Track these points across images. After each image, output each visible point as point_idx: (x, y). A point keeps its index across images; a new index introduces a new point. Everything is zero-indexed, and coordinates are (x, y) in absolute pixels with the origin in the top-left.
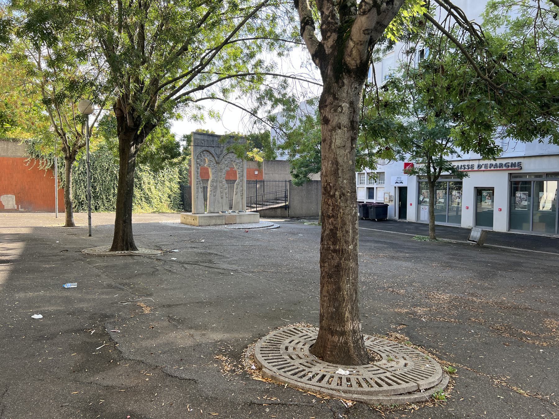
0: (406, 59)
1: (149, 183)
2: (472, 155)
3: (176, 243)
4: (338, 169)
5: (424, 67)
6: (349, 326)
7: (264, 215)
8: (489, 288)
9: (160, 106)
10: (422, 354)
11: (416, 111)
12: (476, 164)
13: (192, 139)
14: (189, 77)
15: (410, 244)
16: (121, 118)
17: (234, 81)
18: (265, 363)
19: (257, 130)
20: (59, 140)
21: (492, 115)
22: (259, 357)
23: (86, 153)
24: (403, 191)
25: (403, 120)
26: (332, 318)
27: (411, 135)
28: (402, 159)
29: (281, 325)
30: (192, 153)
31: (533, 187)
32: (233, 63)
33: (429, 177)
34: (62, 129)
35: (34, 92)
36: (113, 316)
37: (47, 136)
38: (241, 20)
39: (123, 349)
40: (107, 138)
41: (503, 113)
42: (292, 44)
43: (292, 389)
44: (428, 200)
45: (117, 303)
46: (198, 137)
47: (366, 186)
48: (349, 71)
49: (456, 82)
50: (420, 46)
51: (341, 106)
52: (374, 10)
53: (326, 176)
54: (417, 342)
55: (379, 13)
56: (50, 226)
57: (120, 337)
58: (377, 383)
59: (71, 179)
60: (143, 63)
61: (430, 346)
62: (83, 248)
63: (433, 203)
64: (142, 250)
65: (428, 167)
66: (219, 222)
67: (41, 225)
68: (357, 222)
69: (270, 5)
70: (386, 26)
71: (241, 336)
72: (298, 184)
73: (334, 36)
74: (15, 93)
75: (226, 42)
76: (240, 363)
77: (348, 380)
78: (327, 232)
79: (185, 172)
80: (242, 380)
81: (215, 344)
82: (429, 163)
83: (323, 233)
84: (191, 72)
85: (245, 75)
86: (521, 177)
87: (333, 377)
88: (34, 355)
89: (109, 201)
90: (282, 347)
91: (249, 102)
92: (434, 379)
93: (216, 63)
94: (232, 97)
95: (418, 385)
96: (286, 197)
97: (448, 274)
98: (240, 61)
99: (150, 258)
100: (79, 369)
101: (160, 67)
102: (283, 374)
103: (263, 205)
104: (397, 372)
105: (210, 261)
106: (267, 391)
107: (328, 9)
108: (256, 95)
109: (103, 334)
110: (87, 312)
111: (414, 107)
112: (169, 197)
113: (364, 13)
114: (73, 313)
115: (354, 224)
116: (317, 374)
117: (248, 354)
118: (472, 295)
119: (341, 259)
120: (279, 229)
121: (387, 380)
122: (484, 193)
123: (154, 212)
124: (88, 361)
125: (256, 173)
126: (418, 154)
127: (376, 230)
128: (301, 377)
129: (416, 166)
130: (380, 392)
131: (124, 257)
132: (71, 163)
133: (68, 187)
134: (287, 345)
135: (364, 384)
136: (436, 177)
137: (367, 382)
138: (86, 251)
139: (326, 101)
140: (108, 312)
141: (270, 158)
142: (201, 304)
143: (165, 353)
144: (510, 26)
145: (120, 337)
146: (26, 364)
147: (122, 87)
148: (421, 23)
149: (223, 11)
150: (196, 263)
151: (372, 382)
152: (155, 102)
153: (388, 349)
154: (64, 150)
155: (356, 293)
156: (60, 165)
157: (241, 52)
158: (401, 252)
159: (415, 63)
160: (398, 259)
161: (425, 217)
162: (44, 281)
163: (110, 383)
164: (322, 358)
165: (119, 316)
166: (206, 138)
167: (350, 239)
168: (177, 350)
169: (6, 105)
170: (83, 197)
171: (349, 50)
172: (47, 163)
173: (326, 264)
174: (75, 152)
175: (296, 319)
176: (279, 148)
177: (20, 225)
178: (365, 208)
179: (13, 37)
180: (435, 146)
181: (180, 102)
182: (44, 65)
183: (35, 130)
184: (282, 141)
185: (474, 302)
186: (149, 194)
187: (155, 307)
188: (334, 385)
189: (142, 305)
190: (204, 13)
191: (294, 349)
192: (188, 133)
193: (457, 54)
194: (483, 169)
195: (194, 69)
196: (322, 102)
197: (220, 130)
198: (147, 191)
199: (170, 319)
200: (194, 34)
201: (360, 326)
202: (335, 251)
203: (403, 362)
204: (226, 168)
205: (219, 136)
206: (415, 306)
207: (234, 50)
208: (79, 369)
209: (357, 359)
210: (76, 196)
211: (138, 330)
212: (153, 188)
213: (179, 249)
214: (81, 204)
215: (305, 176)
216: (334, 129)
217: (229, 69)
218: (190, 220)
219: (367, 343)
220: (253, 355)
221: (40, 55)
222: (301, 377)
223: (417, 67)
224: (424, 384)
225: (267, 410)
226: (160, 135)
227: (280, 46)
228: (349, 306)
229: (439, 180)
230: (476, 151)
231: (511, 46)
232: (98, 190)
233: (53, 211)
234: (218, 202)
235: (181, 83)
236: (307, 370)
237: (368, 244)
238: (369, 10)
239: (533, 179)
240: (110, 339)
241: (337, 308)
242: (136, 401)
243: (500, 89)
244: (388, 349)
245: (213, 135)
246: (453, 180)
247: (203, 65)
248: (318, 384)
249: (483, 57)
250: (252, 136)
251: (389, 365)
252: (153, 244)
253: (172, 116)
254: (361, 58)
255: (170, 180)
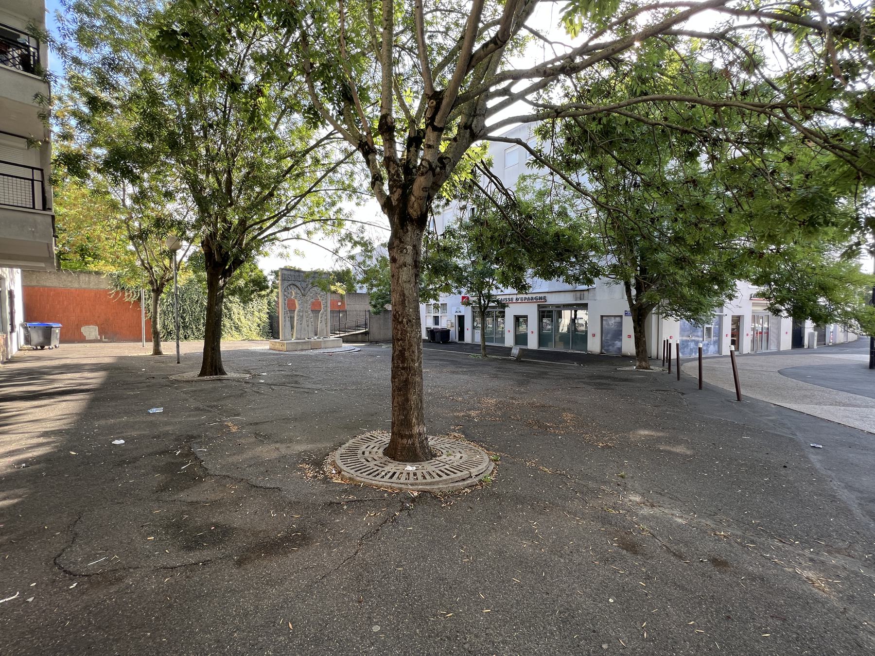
0: (459, 214)
1: (238, 314)
2: (510, 290)
3: (264, 367)
4: (405, 300)
5: (474, 221)
6: (416, 430)
7: (346, 340)
8: (524, 393)
9: (247, 244)
10: (474, 448)
11: (469, 255)
12: (515, 297)
13: (280, 274)
14: (276, 219)
15: (467, 361)
16: (209, 255)
17: (317, 225)
18: (344, 468)
19: (339, 267)
20: (146, 274)
21: (524, 260)
22: (339, 463)
23: (174, 286)
24: (461, 319)
25: (460, 263)
26: (402, 424)
27: (466, 274)
28: (460, 293)
29: (359, 434)
30: (280, 286)
31: (555, 315)
32: (316, 210)
33: (480, 308)
34: (148, 263)
35: (118, 227)
36: (200, 436)
37: (133, 270)
38: (323, 173)
39: (209, 466)
40: (195, 272)
41: (531, 259)
42: (369, 197)
43: (367, 486)
44: (480, 325)
45: (204, 424)
46: (286, 272)
47: (433, 315)
48: (412, 220)
49: (497, 234)
50: (470, 205)
51: (406, 248)
52: (430, 173)
53: (395, 305)
54: (470, 438)
55: (434, 175)
56: (136, 355)
57: (206, 456)
58: (438, 474)
59: (159, 310)
60: (231, 205)
61: (481, 441)
62: (171, 375)
63: (483, 328)
64: (230, 374)
65: (480, 300)
66: (305, 347)
67: (126, 354)
68: (421, 344)
69: (348, 162)
70: (440, 186)
71: (323, 446)
72: (376, 313)
73: (399, 191)
74: (99, 227)
75: (309, 191)
76: (322, 469)
77: (415, 474)
78: (396, 353)
79: (274, 303)
80: (323, 484)
81: (299, 455)
82: (480, 297)
83: (394, 353)
84: (277, 215)
85: (327, 220)
86: (546, 307)
87: (402, 473)
88: (113, 480)
89: (199, 330)
90: (360, 452)
91: (332, 243)
92: (482, 467)
93: (301, 208)
94: (315, 238)
95: (470, 473)
96: (366, 324)
97: (495, 383)
98: (323, 208)
99: (238, 381)
100: (163, 488)
101: (249, 209)
102: (360, 475)
103: (345, 332)
104: (454, 464)
105: (296, 382)
106: (345, 491)
107: (394, 169)
108: (337, 238)
109: (189, 454)
110: (172, 434)
111: (468, 252)
112: (259, 326)
113: (422, 174)
114: (158, 437)
115: (418, 345)
116: (389, 472)
117: (329, 461)
118: (512, 398)
119: (408, 375)
120: (360, 352)
121: (446, 471)
122: (521, 320)
123: (244, 340)
124: (172, 480)
125: (340, 304)
126: (472, 290)
127: (441, 350)
128: (375, 476)
129: (471, 299)
130: (441, 481)
131: (213, 382)
132: (159, 295)
133: (155, 318)
134: (363, 450)
135: (428, 477)
136: (486, 308)
137: (430, 474)
138: (174, 378)
139: (393, 243)
140: (195, 433)
141: (351, 291)
142: (287, 420)
143: (251, 466)
144: (535, 194)
145: (206, 456)
146: (104, 489)
147: (209, 226)
148: (470, 186)
149: (306, 165)
150: (283, 384)
151: (434, 475)
152: (242, 240)
153: (448, 446)
154: (151, 283)
155: (421, 402)
156: (147, 296)
157: (324, 201)
158: (460, 367)
159: (467, 216)
160: (457, 373)
161: (478, 339)
162: (127, 407)
163: (194, 499)
164: (394, 458)
165: (206, 436)
166: (292, 273)
167: (416, 358)
168: (262, 464)
169: (88, 238)
170: (171, 327)
171: (411, 203)
172: (133, 295)
173: (396, 380)
174: (162, 285)
175: (372, 428)
176: (358, 283)
177: (103, 355)
178: (431, 333)
179: (90, 172)
180: (483, 283)
181: (266, 241)
182: (128, 202)
183: (119, 263)
184: (360, 277)
185: (513, 404)
186: (239, 323)
187: (242, 425)
188: (403, 480)
189: (230, 424)
190: (289, 165)
191: (370, 453)
192: (277, 269)
193: (497, 212)
194: (519, 301)
195: (280, 213)
196: (391, 246)
197: (306, 266)
198: (237, 321)
199: (257, 435)
200: (279, 182)
201: (425, 429)
202: (403, 368)
203: (459, 455)
204: (312, 300)
205: (304, 272)
206: (469, 410)
207: (317, 199)
208: (163, 488)
209: (422, 457)
210: (164, 326)
211: (225, 448)
212: (242, 318)
213: (266, 372)
214: (170, 333)
215: (382, 306)
216: (401, 267)
217: (312, 214)
218: (278, 346)
219: (431, 443)
220: (334, 461)
221: (124, 193)
222: (375, 476)
223: (468, 221)
224: (474, 471)
225: (345, 507)
226: (248, 270)
227: (358, 198)
228: (416, 414)
229: (488, 310)
230: (513, 287)
231: (535, 208)
232: (187, 320)
233: (140, 340)
234: (305, 329)
235: (268, 224)
236: (381, 469)
237: (435, 362)
238: (426, 173)
239: (554, 309)
240: (196, 458)
241: (406, 416)
242: (221, 513)
243: (528, 241)
244: (448, 446)
245: (299, 271)
246: (498, 310)
247: (288, 210)
248: (390, 480)
249: (515, 216)
250: (334, 272)
251: (448, 459)
252: (243, 368)
253: (259, 253)
254: (421, 210)
255: (259, 311)
